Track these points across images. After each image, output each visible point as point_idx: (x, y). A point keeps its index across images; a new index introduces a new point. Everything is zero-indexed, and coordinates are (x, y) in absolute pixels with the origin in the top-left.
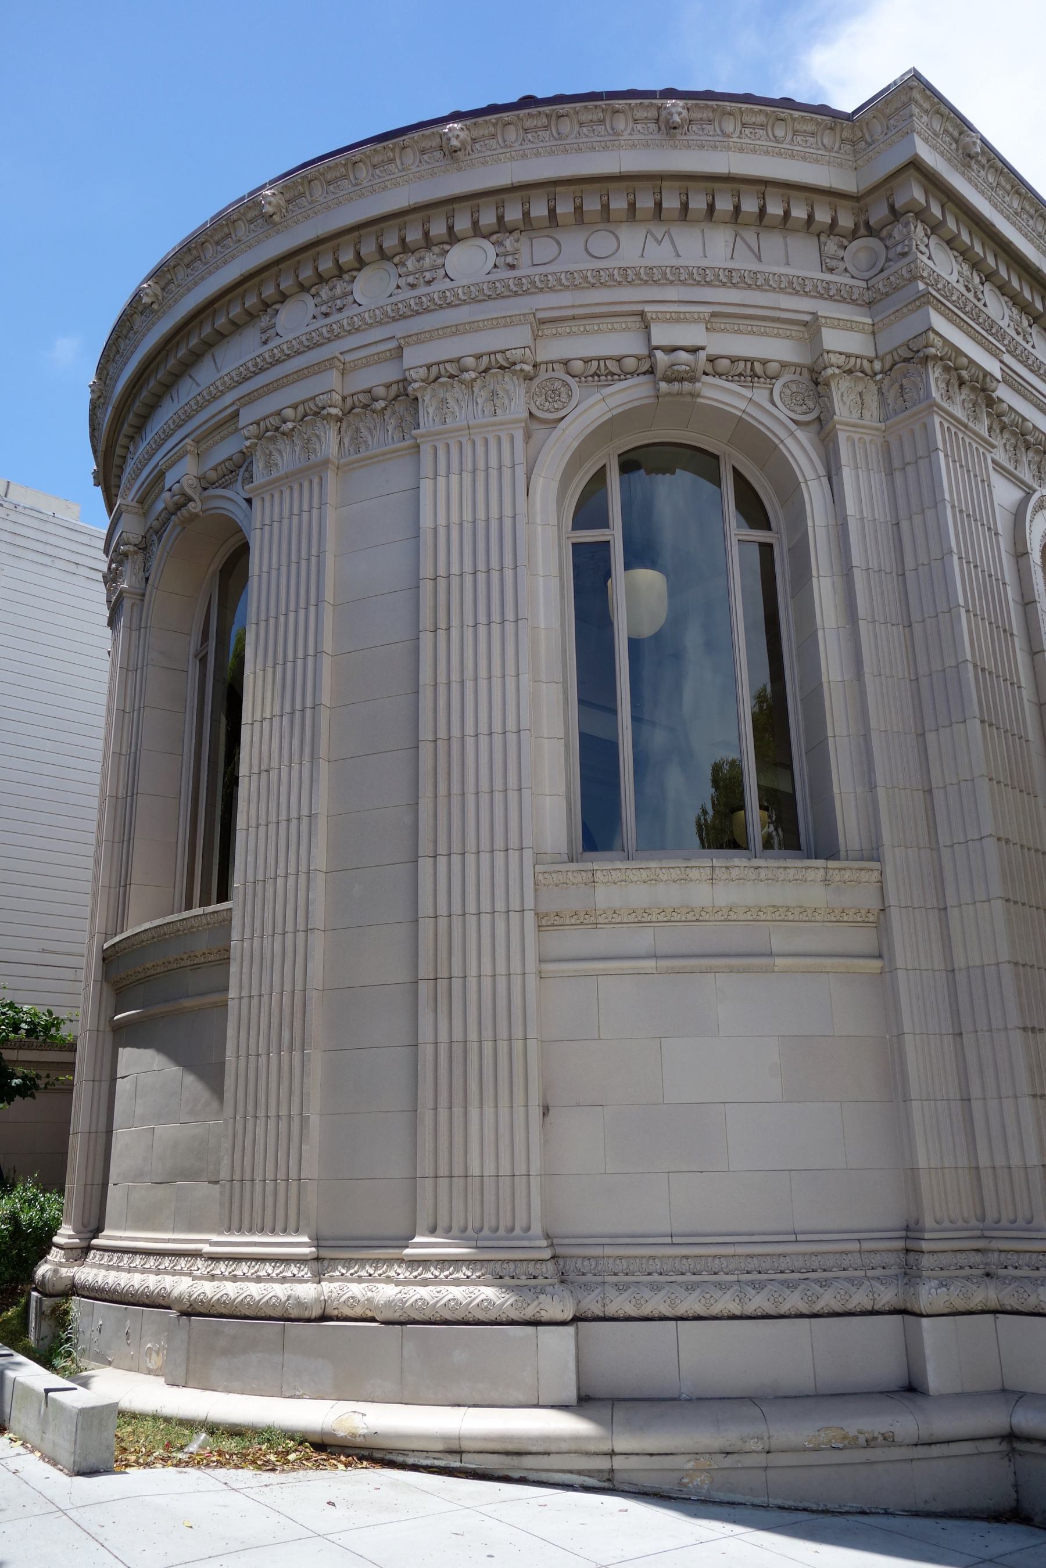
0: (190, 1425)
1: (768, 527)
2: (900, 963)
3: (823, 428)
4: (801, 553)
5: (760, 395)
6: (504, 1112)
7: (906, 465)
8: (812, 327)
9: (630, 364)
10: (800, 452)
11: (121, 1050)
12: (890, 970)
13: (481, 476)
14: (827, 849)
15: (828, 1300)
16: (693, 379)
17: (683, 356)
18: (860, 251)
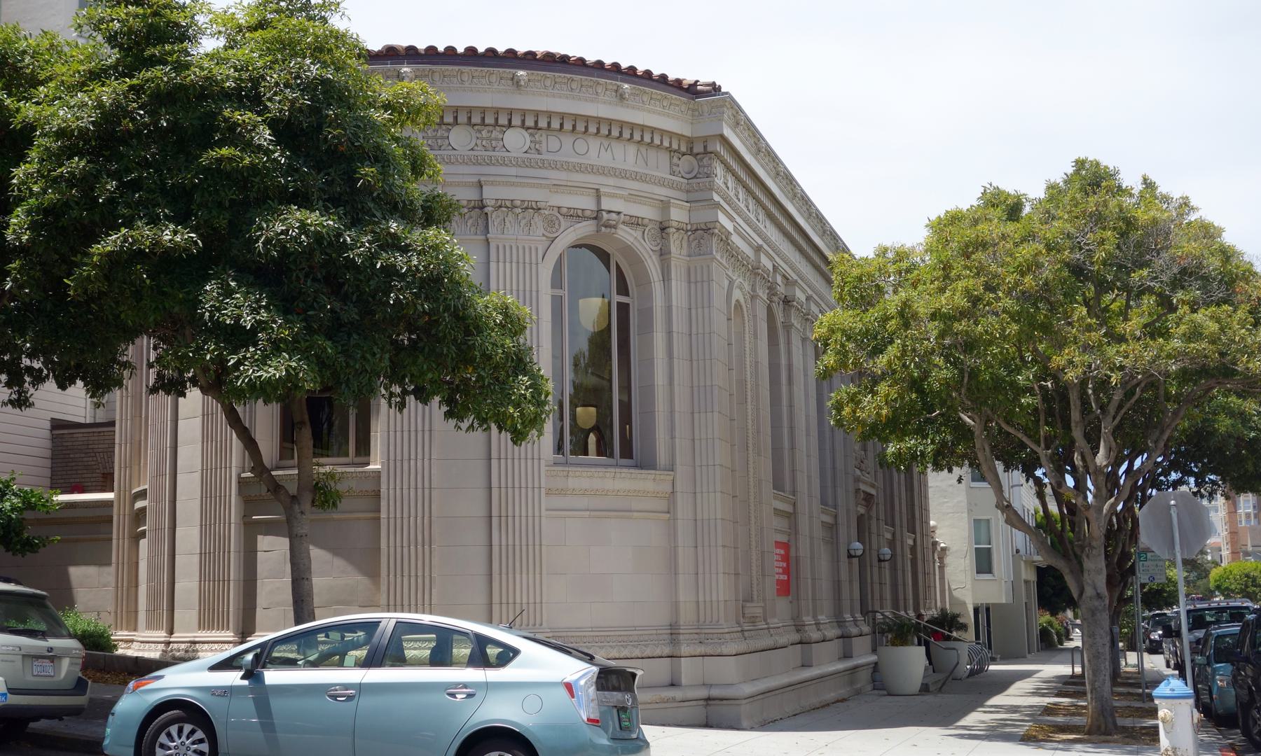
0: (456, 685)
1: (627, 294)
2: (680, 515)
3: (664, 254)
4: (647, 314)
5: (638, 234)
6: (531, 576)
7: (698, 281)
8: (665, 205)
9: (588, 213)
10: (653, 266)
11: (260, 538)
12: (675, 519)
13: (521, 266)
14: (647, 464)
15: (648, 652)
16: (615, 227)
17: (614, 215)
18: (686, 163)
